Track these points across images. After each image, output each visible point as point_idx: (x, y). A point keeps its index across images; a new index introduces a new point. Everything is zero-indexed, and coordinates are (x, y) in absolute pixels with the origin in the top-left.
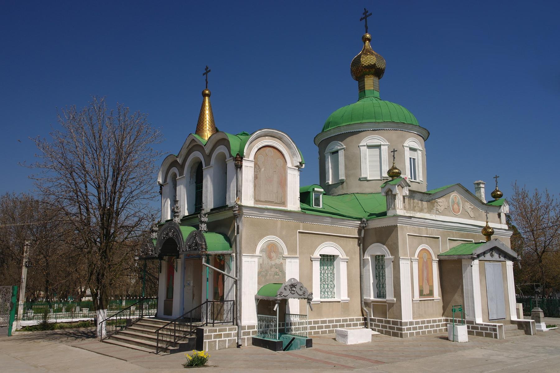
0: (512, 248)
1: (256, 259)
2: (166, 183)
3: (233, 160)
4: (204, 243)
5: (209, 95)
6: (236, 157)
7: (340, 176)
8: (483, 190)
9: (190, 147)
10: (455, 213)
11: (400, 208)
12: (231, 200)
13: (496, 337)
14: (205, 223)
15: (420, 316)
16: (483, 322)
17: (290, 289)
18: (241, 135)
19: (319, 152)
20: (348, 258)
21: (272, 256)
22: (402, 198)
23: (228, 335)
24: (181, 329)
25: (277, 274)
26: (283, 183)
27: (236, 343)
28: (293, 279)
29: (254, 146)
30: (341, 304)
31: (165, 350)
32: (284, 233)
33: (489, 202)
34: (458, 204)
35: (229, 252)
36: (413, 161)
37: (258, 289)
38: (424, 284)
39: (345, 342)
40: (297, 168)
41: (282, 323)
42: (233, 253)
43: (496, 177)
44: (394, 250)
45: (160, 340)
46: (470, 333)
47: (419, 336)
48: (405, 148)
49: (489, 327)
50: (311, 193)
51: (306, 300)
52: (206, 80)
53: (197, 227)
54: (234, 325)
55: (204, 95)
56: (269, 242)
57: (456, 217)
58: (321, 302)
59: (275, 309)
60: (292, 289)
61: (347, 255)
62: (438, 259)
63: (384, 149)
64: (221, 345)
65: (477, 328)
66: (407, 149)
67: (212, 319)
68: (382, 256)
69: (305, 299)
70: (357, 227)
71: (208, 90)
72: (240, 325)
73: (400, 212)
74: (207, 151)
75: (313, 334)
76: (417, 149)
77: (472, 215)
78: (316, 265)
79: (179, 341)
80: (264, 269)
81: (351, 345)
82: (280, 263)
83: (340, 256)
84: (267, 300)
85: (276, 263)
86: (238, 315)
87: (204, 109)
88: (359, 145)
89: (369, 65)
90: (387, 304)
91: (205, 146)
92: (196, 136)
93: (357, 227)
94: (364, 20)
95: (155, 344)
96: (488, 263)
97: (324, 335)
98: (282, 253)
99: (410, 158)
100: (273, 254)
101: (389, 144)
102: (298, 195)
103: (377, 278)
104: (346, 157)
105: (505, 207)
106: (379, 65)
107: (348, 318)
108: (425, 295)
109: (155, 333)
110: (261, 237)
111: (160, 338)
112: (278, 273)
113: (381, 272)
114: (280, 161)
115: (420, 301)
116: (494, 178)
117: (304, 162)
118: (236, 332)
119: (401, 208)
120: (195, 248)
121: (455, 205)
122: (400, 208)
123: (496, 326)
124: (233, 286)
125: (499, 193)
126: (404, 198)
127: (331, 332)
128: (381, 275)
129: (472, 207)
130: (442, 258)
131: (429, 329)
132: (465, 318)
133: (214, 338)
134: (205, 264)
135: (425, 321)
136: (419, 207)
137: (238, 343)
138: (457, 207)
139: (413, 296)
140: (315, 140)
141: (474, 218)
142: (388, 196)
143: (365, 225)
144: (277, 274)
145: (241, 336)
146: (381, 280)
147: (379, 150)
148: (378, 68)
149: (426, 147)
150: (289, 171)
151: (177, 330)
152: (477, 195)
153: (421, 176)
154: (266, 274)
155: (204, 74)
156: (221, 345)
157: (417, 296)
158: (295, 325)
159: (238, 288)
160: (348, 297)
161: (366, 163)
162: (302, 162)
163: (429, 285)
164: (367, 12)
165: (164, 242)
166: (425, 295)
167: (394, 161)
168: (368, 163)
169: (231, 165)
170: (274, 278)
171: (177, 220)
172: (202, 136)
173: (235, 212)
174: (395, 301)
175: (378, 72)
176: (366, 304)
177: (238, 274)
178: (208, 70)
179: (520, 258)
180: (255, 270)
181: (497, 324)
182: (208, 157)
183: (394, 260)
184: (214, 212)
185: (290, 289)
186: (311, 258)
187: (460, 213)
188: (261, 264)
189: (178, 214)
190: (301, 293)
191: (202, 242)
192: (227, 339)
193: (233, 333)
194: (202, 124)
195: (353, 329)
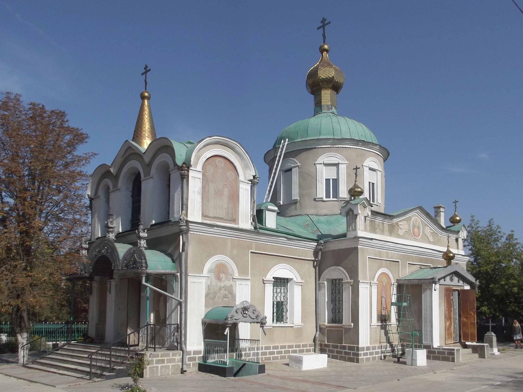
1: (203, 280)
2: (97, 196)
4: (144, 261)
5: (148, 98)
6: (182, 166)
9: (126, 155)
10: (414, 236)
11: (361, 229)
12: (176, 214)
13: (453, 360)
14: (144, 238)
17: (242, 312)
18: (187, 143)
20: (303, 281)
22: (363, 218)
24: (117, 354)
25: (227, 297)
26: (235, 198)
28: (246, 301)
31: (101, 376)
32: (235, 252)
34: (419, 228)
35: (173, 271)
39: (300, 368)
42: (177, 273)
43: (456, 202)
44: (354, 273)
45: (93, 365)
46: (428, 357)
49: (446, 351)
50: (264, 211)
51: (259, 324)
52: (145, 81)
53: (135, 244)
55: (143, 98)
57: (416, 241)
58: (273, 327)
59: (225, 333)
60: (244, 312)
61: (302, 279)
63: (343, 168)
65: (434, 352)
66: (366, 169)
67: (154, 344)
68: (339, 280)
69: (257, 323)
70: (313, 249)
72: (185, 350)
73: (360, 234)
74: (147, 159)
75: (272, 359)
76: (377, 170)
77: (431, 239)
78: (269, 288)
79: (115, 367)
82: (229, 285)
83: (295, 279)
85: (226, 285)
86: (183, 339)
89: (327, 78)
92: (133, 143)
93: (313, 249)
94: (322, 29)
95: (88, 370)
97: (275, 361)
100: (222, 276)
101: (348, 163)
104: (301, 175)
106: (336, 79)
109: (88, 357)
110: (210, 256)
111: (93, 363)
112: (227, 295)
113: (338, 296)
114: (231, 174)
115: (378, 325)
118: (181, 357)
122: (361, 229)
123: (454, 350)
124: (176, 307)
125: (458, 218)
126: (365, 219)
127: (283, 358)
128: (337, 299)
129: (432, 231)
130: (401, 282)
132: (422, 343)
133: (156, 364)
134: (145, 284)
139: (371, 322)
140: (265, 157)
141: (434, 243)
142: (348, 217)
144: (227, 297)
146: (337, 305)
147: (337, 167)
148: (336, 82)
149: (385, 168)
150: (241, 186)
151: (113, 355)
155: (142, 74)
158: (245, 351)
159: (183, 311)
160: (302, 322)
162: (255, 176)
164: (326, 20)
165: (96, 259)
167: (356, 178)
169: (175, 176)
171: (112, 236)
172: (140, 143)
173: (182, 227)
174: (352, 326)
175: (336, 87)
176: (320, 329)
178: (148, 69)
179: (478, 283)
183: (353, 283)
184: (154, 227)
185: (242, 313)
186: (263, 280)
187: (419, 237)
188: (209, 286)
189: (112, 230)
190: (253, 316)
191: (142, 260)
193: (177, 359)
194: (140, 129)
195: (306, 354)
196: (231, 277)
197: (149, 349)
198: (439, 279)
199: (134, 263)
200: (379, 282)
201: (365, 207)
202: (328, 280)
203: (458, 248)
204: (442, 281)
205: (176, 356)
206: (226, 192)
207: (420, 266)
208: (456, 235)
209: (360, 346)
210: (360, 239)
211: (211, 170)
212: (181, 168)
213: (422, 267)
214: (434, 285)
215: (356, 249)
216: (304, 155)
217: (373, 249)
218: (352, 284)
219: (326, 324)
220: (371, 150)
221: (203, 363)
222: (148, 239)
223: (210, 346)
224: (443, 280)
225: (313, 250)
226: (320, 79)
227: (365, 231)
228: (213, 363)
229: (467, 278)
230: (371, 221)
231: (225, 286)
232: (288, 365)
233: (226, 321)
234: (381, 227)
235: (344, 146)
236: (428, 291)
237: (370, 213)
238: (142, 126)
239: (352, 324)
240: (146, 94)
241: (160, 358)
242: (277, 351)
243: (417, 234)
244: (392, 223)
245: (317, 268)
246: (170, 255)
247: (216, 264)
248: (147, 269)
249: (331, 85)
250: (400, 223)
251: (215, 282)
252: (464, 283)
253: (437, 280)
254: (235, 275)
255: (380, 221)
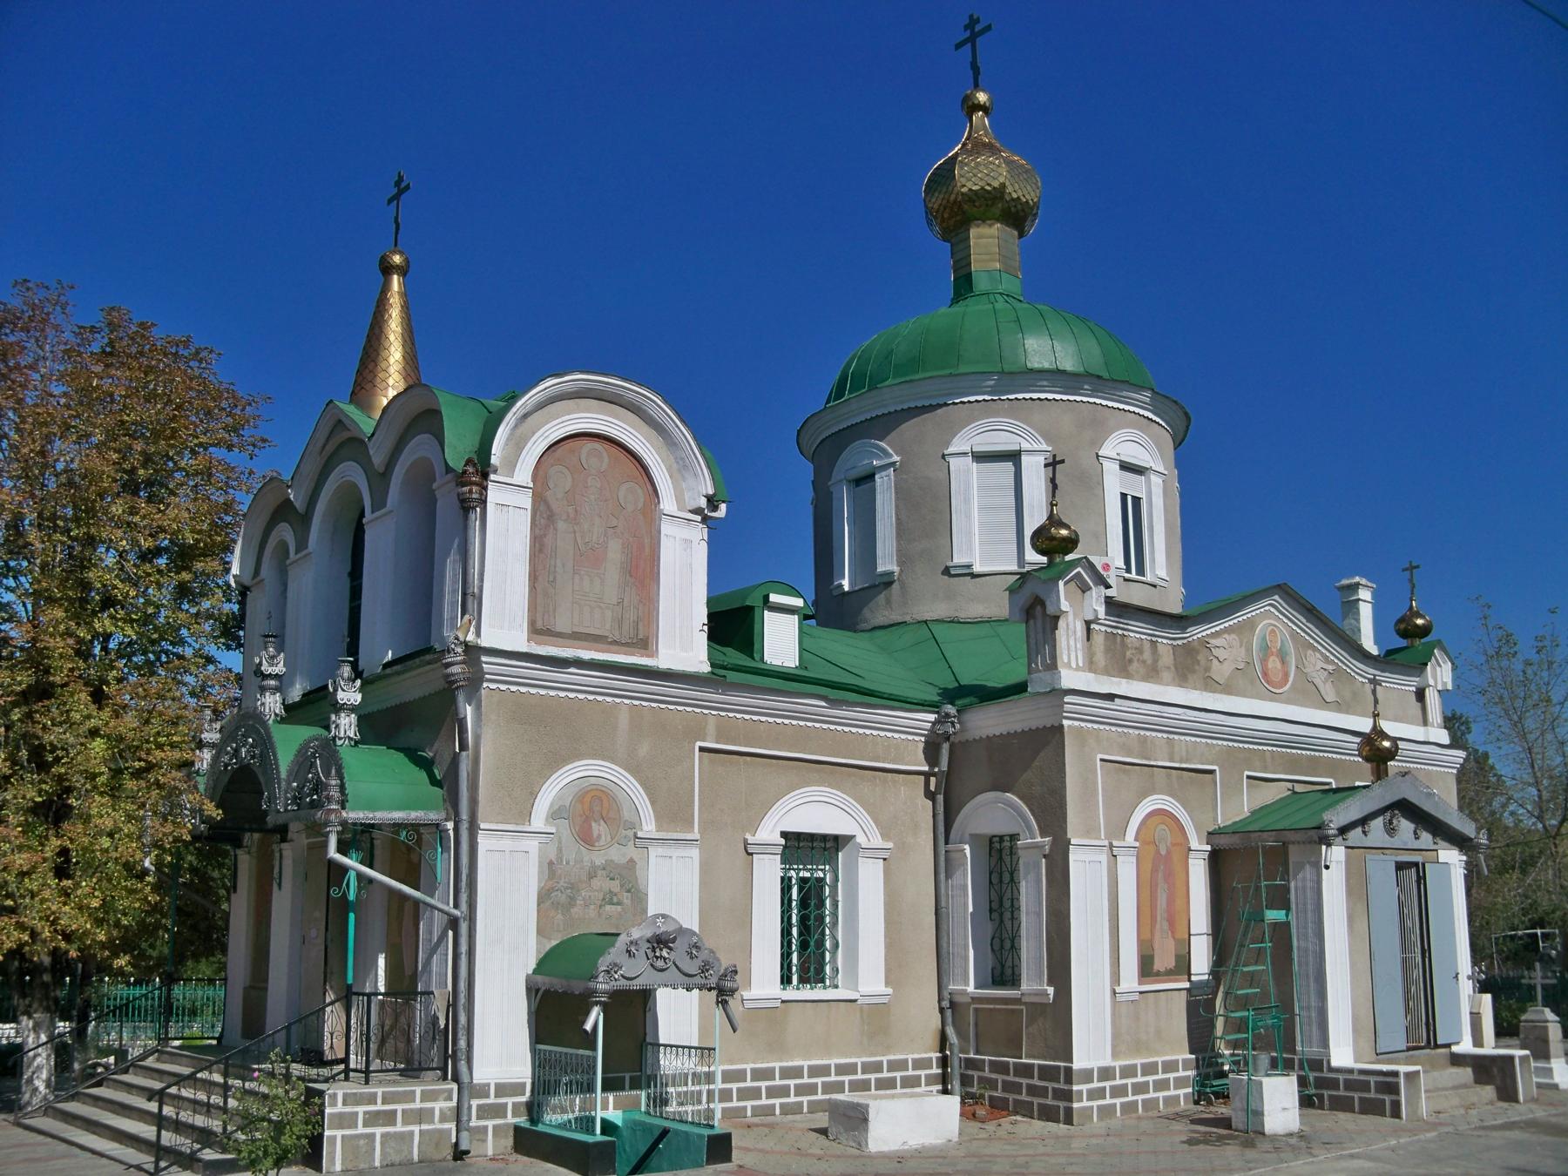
0: (1461, 808)
3: (454, 484)
4: (333, 782)
6: (465, 472)
7: (879, 561)
8: (1366, 612)
9: (330, 448)
10: (1268, 686)
11: (1074, 665)
12: (455, 631)
13: (1396, 1113)
15: (1138, 1047)
16: (1356, 1062)
19: (813, 482)
20: (890, 845)
21: (595, 834)
22: (1080, 627)
23: (421, 1116)
25: (615, 900)
27: (449, 1145)
28: (664, 916)
29: (534, 433)
30: (862, 1010)
33: (1389, 653)
35: (433, 816)
36: (1132, 508)
37: (538, 951)
38: (1157, 935)
40: (699, 518)
41: (631, 1078)
42: (446, 820)
43: (1412, 568)
44: (1052, 815)
46: (1306, 1102)
47: (1134, 1115)
48: (1107, 464)
49: (1372, 1079)
50: (757, 612)
51: (714, 993)
54: (445, 1078)
55: (387, 269)
56: (585, 783)
57: (1276, 701)
58: (783, 1002)
59: (588, 1026)
60: (657, 954)
62: (1209, 848)
64: (392, 1151)
65: (1333, 1084)
71: (401, 253)
72: (465, 1078)
74: (378, 458)
76: (1147, 469)
80: (562, 883)
81: (900, 1158)
82: (624, 861)
83: (861, 839)
84: (565, 993)
85: (611, 861)
86: (462, 1043)
87: (383, 316)
88: (946, 452)
90: (1023, 1007)
91: (370, 438)
96: (1376, 857)
98: (631, 826)
99: (1124, 496)
100: (599, 828)
102: (701, 615)
103: (995, 915)
104: (903, 495)
105: (1438, 669)
107: (885, 1059)
108: (1158, 974)
113: (1008, 895)
114: (630, 494)
115: (1141, 993)
116: (1404, 570)
117: (723, 495)
118: (454, 1103)
119: (1077, 664)
120: (312, 801)
121: (1272, 659)
122: (1074, 665)
123: (1395, 1074)
124: (443, 936)
125: (1420, 622)
126: (1089, 630)
128: (1007, 904)
129: (1330, 668)
130: (1224, 841)
131: (1172, 1092)
132: (1294, 1052)
133: (365, 1125)
135: (1157, 1063)
136: (1144, 662)
137: (456, 1144)
138: (1279, 665)
139: (1116, 978)
141: (1339, 706)
142: (1032, 622)
143: (954, 727)
144: (615, 900)
145: (470, 1119)
146: (1008, 924)
150: (667, 528)
152: (1346, 625)
153: (1162, 562)
154: (572, 899)
155: (390, 201)
156: (392, 1151)
157: (1130, 980)
159: (464, 948)
161: (969, 517)
162: (714, 495)
163: (1174, 938)
164: (978, 21)
166: (1158, 974)
168: (976, 515)
170: (600, 915)
173: (450, 670)
174: (1051, 997)
176: (951, 1007)
177: (464, 897)
178: (403, 185)
180: (530, 882)
181: (1403, 1069)
182: (380, 479)
183: (1051, 850)
185: (651, 955)
186: (746, 843)
188: (551, 863)
190: (692, 967)
192: (416, 1129)
195: (882, 1097)
196: (630, 833)
197: (351, 1074)
198: (1343, 831)
199: (315, 790)
200: (1144, 843)
201: (1085, 589)
202: (975, 839)
203: (1425, 723)
204: (1355, 835)
205: (435, 1100)
206: (615, 552)
207: (1289, 785)
208: (1417, 679)
209: (1077, 1064)
210: (1067, 699)
211: (561, 480)
212: (461, 479)
213: (1296, 790)
214: (1324, 847)
215: (1060, 729)
216: (909, 428)
217: (1120, 730)
218: (1047, 852)
219: (971, 988)
220: (1127, 407)
221: (527, 1125)
222: (362, 712)
223: (550, 1068)
224: (1359, 830)
225: (923, 739)
226: (963, 194)
227: (1090, 670)
228: (563, 1126)
229: (1446, 824)
230: (1110, 637)
231: (609, 862)
232: (823, 1132)
233: (591, 985)
234: (1147, 655)
235: (1035, 396)
236: (1308, 872)
237: (1101, 610)
238: (379, 354)
239: (1051, 990)
240: (397, 259)
241: (379, 1107)
242: (795, 1085)
243: (1277, 678)
244: (1185, 641)
245: (940, 798)
246: (426, 765)
247: (577, 789)
248: (343, 808)
249: (997, 209)
250: (1213, 642)
251: (573, 849)
252: (1438, 840)
253: (1331, 832)
254: (644, 823)
255: (1143, 637)
